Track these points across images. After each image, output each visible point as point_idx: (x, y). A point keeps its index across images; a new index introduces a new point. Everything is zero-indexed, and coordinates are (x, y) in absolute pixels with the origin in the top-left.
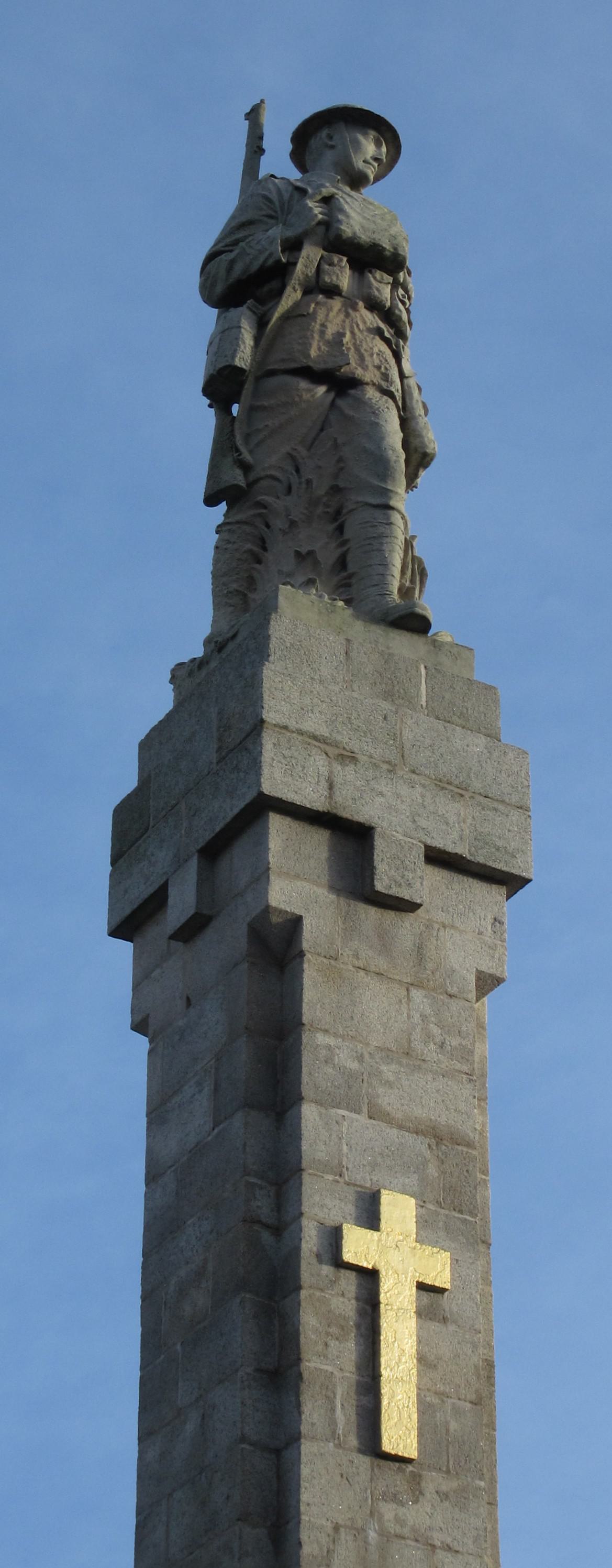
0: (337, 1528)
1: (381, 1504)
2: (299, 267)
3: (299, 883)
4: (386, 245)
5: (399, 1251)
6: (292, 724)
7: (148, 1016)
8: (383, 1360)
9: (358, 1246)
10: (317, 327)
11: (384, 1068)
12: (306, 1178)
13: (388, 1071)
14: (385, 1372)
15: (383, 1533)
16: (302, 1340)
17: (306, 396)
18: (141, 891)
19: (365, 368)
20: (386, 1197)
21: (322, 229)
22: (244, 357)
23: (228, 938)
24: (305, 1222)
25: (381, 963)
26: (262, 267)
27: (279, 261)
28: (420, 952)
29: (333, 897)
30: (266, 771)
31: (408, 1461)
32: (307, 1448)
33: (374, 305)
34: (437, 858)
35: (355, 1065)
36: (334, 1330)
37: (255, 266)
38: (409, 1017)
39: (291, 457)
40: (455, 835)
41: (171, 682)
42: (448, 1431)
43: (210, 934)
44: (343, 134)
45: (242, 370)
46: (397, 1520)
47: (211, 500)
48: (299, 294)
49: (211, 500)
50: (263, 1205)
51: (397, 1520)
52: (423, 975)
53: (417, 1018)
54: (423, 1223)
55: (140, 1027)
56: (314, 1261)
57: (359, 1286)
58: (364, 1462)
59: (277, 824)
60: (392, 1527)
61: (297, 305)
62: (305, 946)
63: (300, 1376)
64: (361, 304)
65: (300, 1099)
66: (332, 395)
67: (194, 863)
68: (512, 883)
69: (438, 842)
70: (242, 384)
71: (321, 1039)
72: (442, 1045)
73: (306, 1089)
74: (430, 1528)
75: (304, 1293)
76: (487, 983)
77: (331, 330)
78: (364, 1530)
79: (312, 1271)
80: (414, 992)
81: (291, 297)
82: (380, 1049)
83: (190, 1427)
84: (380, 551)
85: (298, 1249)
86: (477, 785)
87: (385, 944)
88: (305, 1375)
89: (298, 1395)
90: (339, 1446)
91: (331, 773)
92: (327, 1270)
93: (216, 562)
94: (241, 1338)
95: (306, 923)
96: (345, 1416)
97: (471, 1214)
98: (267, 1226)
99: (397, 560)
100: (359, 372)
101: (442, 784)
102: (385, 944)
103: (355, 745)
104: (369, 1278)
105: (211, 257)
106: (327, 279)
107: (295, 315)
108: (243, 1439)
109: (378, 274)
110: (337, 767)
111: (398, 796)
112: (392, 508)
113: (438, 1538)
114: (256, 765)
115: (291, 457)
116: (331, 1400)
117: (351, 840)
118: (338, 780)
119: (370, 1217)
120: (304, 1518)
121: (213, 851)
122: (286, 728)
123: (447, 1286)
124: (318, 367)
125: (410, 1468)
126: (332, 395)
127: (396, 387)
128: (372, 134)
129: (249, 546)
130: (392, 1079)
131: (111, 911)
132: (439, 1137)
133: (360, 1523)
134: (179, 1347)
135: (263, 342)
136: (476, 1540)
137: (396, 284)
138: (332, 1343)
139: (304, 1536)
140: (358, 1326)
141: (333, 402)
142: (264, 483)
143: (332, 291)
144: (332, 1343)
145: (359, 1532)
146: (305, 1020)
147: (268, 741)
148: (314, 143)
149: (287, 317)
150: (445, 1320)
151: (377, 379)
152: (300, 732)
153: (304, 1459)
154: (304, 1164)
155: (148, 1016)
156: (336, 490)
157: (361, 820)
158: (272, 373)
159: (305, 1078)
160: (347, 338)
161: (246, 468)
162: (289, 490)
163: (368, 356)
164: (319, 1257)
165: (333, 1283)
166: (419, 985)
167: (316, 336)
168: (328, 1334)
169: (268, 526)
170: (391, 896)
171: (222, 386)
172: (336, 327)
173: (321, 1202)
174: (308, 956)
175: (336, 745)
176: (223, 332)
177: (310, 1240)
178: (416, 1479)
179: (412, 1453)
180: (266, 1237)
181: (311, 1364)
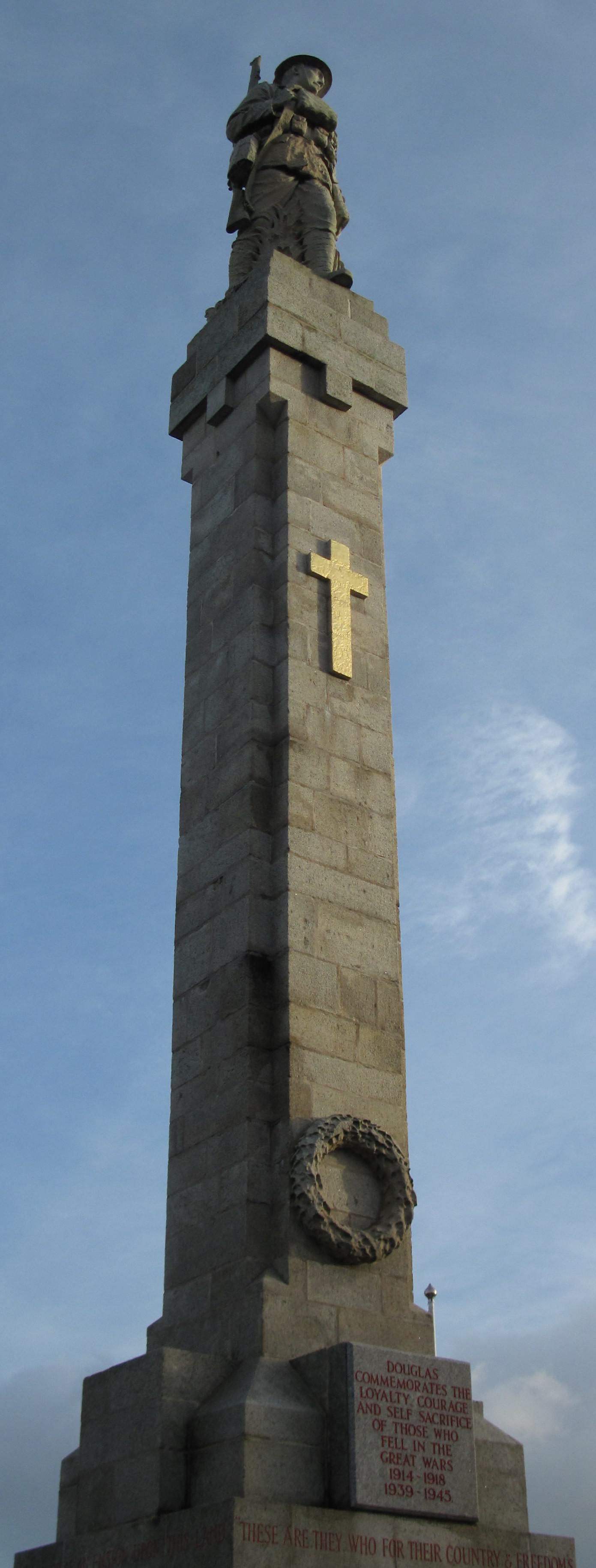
0: (308, 706)
1: (332, 698)
2: (282, 118)
3: (286, 385)
4: (327, 114)
5: (340, 570)
6: (283, 306)
7: (192, 470)
8: (333, 624)
9: (318, 565)
10: (290, 148)
11: (331, 482)
12: (290, 527)
13: (334, 485)
14: (334, 631)
15: (333, 713)
16: (289, 607)
17: (283, 180)
18: (189, 405)
19: (315, 171)
20: (334, 544)
21: (293, 103)
22: (252, 154)
23: (246, 413)
24: (290, 549)
25: (329, 431)
26: (262, 117)
27: (271, 114)
28: (349, 431)
29: (303, 395)
30: (269, 324)
31: (345, 678)
32: (291, 662)
33: (319, 144)
34: (360, 388)
35: (316, 478)
36: (306, 606)
37: (258, 118)
38: (344, 461)
39: (275, 208)
40: (368, 377)
41: (206, 316)
42: (367, 669)
43: (232, 418)
44: (303, 69)
45: (250, 162)
46: (341, 707)
47: (230, 229)
48: (281, 132)
49: (230, 229)
50: (264, 542)
51: (341, 707)
52: (350, 440)
53: (348, 462)
54: (353, 563)
55: (187, 477)
56: (295, 569)
57: (319, 586)
58: (323, 676)
59: (275, 358)
60: (338, 712)
61: (279, 137)
62: (289, 415)
63: (288, 625)
64: (313, 142)
65: (286, 488)
66: (296, 183)
67: (224, 381)
68: (397, 409)
69: (359, 379)
70: (249, 172)
71: (297, 461)
72: (361, 478)
73: (290, 484)
74: (359, 715)
75: (289, 584)
76: (385, 455)
77: (297, 151)
78: (323, 710)
79: (294, 575)
80: (346, 450)
81: (277, 133)
82: (330, 473)
83: (219, 662)
84: (324, 251)
85: (285, 564)
86: (378, 357)
87: (331, 424)
88: (291, 625)
89: (286, 635)
90: (309, 664)
91: (304, 333)
92: (302, 575)
93: (232, 260)
94: (253, 606)
95: (289, 404)
96: (313, 651)
97: (378, 563)
98: (267, 554)
99: (332, 256)
100: (312, 172)
101: (360, 353)
102: (331, 424)
103: (315, 324)
104: (325, 583)
105: (233, 116)
106: (296, 126)
107: (277, 142)
108: (254, 658)
109: (322, 130)
110: (307, 332)
111: (339, 353)
112: (330, 231)
113: (363, 721)
114: (264, 322)
115: (275, 209)
116: (304, 640)
117: (314, 369)
118: (307, 338)
119: (325, 551)
120: (290, 698)
121: (234, 376)
122: (279, 307)
123: (367, 595)
124: (290, 166)
125: (347, 683)
126: (296, 183)
127: (330, 183)
128: (318, 71)
129: (250, 251)
130: (336, 489)
131: (170, 423)
132: (361, 523)
133: (320, 707)
134: (212, 623)
135: (262, 151)
136: (383, 727)
137: (330, 137)
138: (305, 612)
139: (290, 707)
140: (319, 607)
141: (297, 186)
142: (259, 220)
143: (298, 133)
144: (305, 612)
145: (320, 711)
146: (289, 450)
147: (271, 312)
148: (287, 74)
149: (275, 142)
150: (365, 613)
151: (321, 177)
152: (287, 311)
153: (290, 668)
154: (289, 520)
155: (192, 470)
156: (299, 222)
157: (319, 359)
158: (265, 168)
159: (289, 479)
160: (306, 155)
161: (251, 212)
162: (273, 226)
163: (316, 167)
164: (297, 567)
165: (306, 582)
166: (349, 447)
167: (290, 153)
168: (302, 607)
169: (261, 242)
170: (335, 399)
171: (239, 175)
172: (301, 150)
173: (298, 542)
174: (290, 420)
175: (306, 321)
176: (251, 102)
177: (292, 559)
178: (351, 691)
179: (349, 674)
180: (266, 559)
181: (294, 620)
